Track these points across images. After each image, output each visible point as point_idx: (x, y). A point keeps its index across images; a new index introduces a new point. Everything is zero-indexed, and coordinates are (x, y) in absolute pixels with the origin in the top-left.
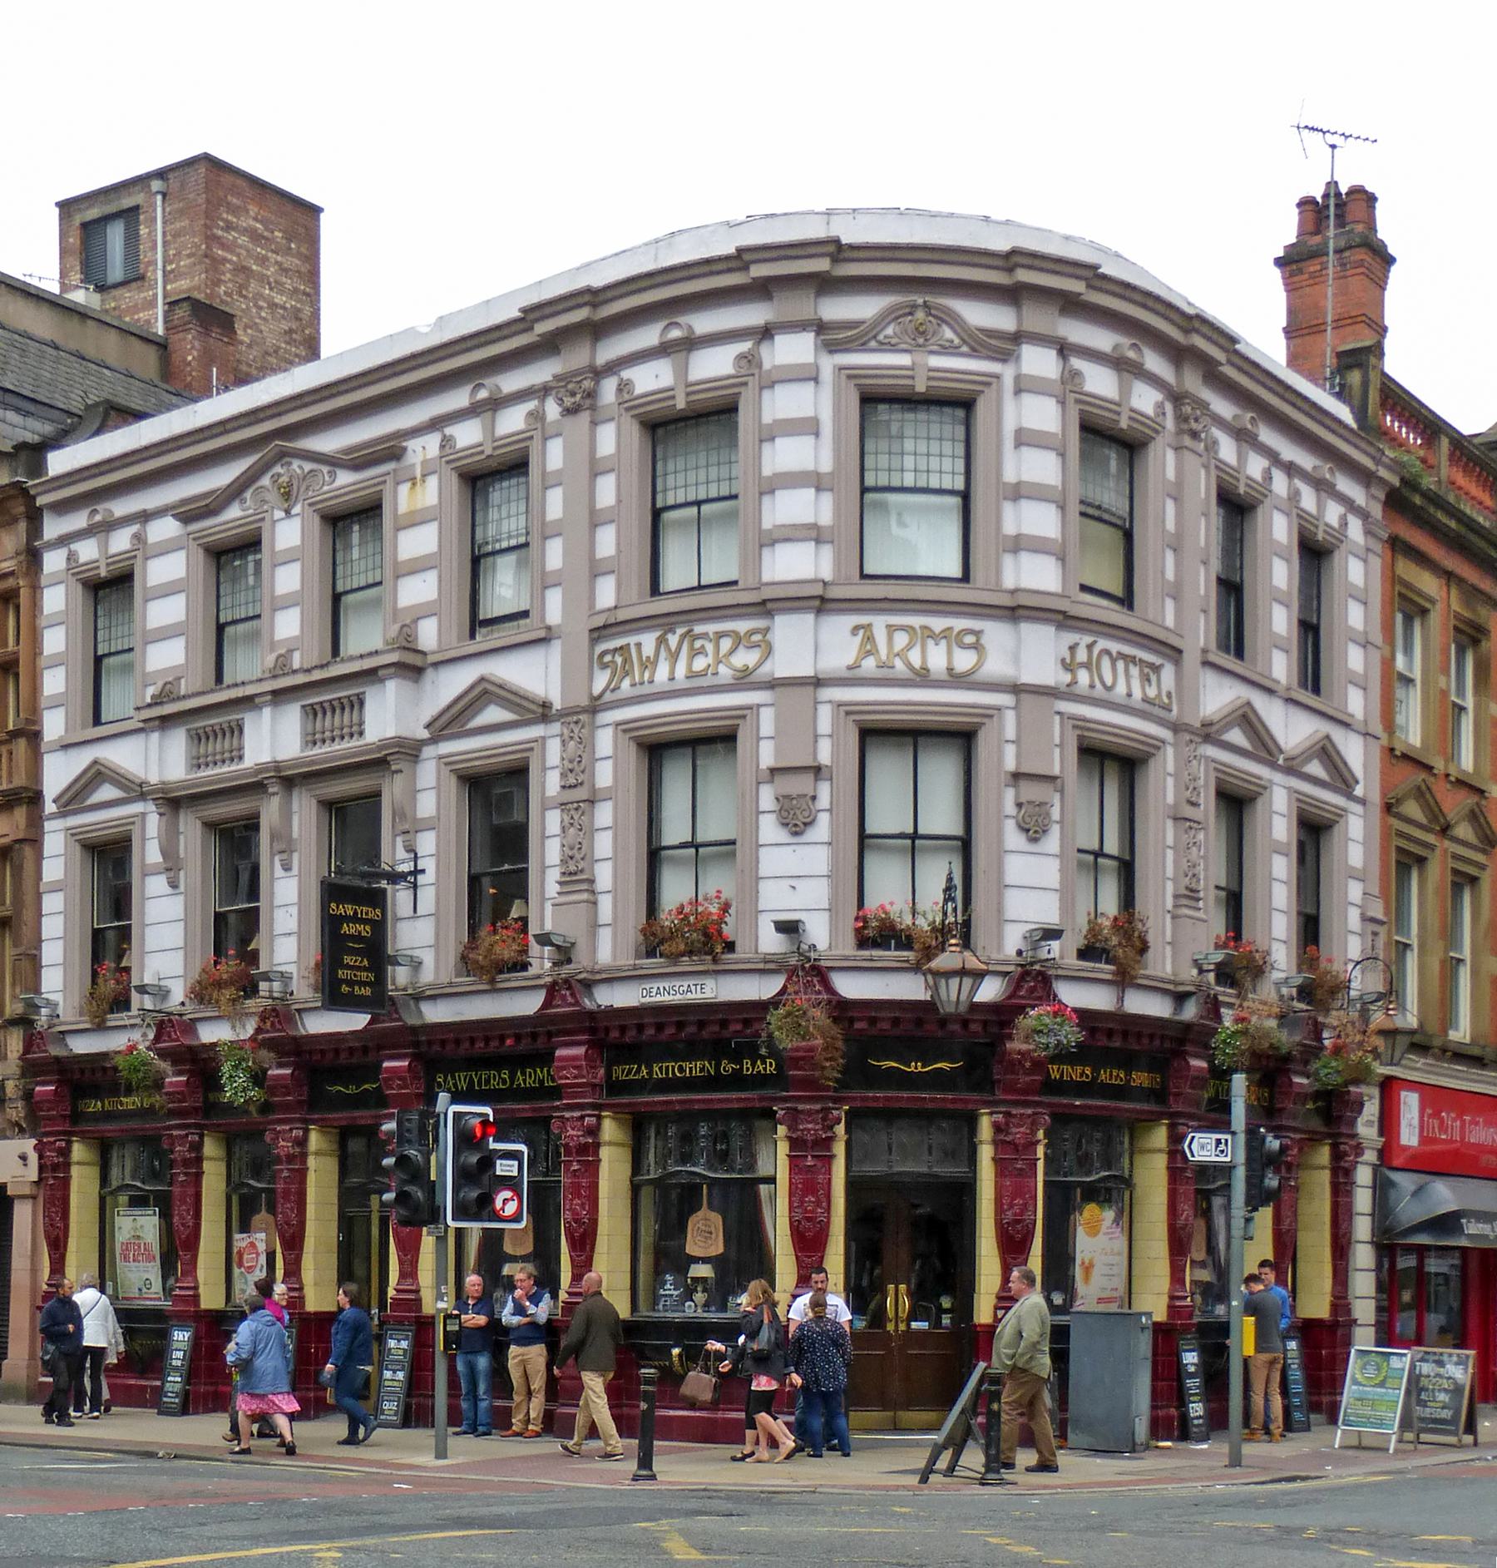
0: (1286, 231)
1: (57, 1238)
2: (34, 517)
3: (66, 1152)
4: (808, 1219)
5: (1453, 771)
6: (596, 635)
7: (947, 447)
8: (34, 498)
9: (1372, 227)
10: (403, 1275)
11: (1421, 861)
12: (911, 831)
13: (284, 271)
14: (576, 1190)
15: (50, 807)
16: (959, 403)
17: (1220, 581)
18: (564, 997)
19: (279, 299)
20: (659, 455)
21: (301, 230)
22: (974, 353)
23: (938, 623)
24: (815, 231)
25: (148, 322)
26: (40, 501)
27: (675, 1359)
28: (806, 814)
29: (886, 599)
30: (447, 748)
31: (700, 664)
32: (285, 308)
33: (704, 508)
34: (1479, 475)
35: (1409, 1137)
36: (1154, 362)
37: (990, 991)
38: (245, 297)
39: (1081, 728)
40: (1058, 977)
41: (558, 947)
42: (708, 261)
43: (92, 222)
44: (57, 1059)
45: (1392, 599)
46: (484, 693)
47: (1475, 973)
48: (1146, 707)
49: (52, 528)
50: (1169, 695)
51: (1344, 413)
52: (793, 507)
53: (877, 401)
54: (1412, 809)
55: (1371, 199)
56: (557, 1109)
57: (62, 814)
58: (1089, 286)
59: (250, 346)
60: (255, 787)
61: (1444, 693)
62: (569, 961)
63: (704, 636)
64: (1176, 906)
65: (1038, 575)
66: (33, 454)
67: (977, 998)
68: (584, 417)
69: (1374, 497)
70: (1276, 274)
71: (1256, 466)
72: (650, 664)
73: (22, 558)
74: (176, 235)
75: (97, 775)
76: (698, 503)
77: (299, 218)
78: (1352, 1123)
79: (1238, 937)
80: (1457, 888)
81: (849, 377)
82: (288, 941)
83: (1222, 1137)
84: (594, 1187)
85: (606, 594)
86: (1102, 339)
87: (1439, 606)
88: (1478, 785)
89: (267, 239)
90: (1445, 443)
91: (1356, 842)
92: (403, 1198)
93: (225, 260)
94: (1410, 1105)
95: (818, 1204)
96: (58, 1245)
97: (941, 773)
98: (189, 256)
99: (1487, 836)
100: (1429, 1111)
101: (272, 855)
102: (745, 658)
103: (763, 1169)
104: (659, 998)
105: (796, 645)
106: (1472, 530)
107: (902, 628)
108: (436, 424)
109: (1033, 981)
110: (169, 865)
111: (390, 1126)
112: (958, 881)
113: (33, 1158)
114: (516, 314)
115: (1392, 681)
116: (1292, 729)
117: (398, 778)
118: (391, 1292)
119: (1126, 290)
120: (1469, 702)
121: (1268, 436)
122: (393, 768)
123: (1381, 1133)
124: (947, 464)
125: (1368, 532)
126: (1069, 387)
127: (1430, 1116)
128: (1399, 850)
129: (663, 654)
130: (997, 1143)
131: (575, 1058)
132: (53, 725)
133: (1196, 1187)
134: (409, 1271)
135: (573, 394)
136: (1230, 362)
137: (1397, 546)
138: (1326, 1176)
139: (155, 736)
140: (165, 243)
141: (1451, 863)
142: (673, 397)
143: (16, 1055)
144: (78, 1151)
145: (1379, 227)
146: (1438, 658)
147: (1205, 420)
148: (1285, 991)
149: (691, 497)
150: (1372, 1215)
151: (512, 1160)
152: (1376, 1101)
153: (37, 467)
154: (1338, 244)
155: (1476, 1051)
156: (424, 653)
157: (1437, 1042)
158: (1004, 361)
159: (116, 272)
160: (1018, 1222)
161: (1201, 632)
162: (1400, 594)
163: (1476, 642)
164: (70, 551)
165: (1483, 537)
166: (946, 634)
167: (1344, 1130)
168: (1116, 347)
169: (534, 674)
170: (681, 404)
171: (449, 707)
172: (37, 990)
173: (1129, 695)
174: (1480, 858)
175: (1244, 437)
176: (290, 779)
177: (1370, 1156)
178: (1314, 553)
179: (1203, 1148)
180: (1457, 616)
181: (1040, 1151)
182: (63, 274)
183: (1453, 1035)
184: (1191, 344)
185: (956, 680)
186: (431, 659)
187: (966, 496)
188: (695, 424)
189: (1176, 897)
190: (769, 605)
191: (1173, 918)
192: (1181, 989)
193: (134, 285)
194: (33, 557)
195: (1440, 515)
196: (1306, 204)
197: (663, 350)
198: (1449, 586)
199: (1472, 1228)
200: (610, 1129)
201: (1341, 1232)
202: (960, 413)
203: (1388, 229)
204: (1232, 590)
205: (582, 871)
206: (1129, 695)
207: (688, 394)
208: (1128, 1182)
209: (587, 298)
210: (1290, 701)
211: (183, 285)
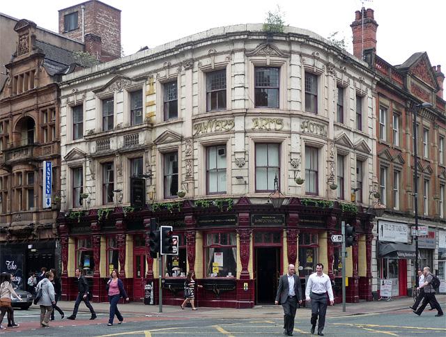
0: (353, 18)
2: (59, 91)
9: (373, 18)
12: (266, 165)
14: (190, 249)
15: (63, 159)
22: (280, 56)
26: (61, 87)
36: (321, 56)
49: (64, 93)
54: (384, 156)
55: (373, 11)
60: (113, 155)
66: (59, 76)
68: (191, 70)
70: (351, 29)
71: (345, 78)
79: (342, 121)
80: (395, 174)
84: (194, 248)
85: (196, 111)
86: (309, 52)
91: (371, 166)
93: (99, 24)
97: (273, 154)
102: (228, 127)
103: (233, 244)
105: (239, 124)
112: (278, 177)
115: (380, 127)
119: (315, 41)
120: (397, 130)
130: (287, 237)
132: (64, 141)
133: (334, 250)
134: (151, 268)
137: (379, 94)
138: (365, 243)
144: (198, 235)
151: (176, 239)
154: (365, 22)
159: (72, 28)
161: (333, 118)
164: (68, 97)
169: (177, 129)
174: (401, 166)
176: (121, 153)
178: (360, 97)
179: (335, 238)
184: (333, 51)
185: (277, 131)
194: (59, 101)
200: (198, 235)
202: (277, 69)
203: (376, 18)
204: (341, 108)
208: (318, 246)
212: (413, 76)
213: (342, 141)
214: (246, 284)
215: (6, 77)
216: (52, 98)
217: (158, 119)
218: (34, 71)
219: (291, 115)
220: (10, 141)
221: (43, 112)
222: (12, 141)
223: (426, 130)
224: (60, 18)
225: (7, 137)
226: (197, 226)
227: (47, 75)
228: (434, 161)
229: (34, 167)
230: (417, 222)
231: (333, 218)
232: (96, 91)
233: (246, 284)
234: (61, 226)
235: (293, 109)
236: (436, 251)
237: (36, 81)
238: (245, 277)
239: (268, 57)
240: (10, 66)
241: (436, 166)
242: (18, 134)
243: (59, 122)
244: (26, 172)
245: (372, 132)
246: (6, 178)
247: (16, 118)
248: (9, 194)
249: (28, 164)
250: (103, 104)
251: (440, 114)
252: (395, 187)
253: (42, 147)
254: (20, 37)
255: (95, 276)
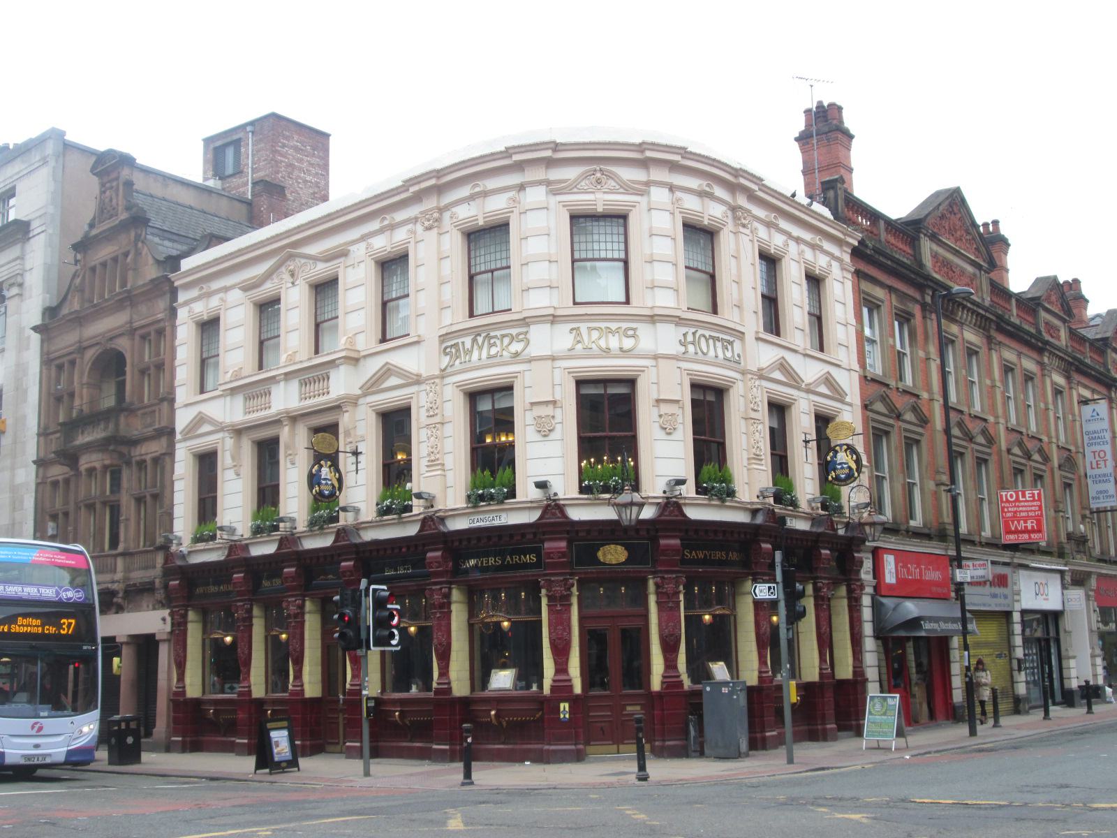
1: (180, 662)
2: (174, 292)
3: (185, 616)
4: (559, 639)
5: (900, 385)
6: (442, 338)
7: (615, 238)
8: (173, 283)
9: (841, 122)
10: (354, 676)
11: (887, 433)
13: (311, 165)
15: (178, 437)
16: (620, 218)
17: (763, 296)
18: (430, 526)
19: (308, 178)
20: (472, 248)
21: (320, 145)
23: (614, 326)
24: (546, 139)
25: (244, 192)
27: (493, 718)
28: (549, 425)
29: (586, 315)
30: (370, 399)
31: (493, 351)
32: (311, 182)
33: (495, 273)
34: (903, 238)
35: (890, 578)
36: (719, 192)
37: (648, 513)
38: (291, 178)
39: (691, 375)
40: (685, 504)
41: (426, 499)
42: (492, 154)
43: (221, 150)
44: (180, 567)
45: (860, 301)
46: (387, 371)
47: (922, 489)
48: (728, 363)
49: (182, 297)
50: (739, 356)
51: (826, 212)
52: (538, 273)
53: (580, 219)
54: (879, 406)
56: (429, 584)
57: (185, 440)
58: (682, 157)
59: (293, 201)
60: (277, 422)
61: (894, 346)
62: (432, 506)
63: (495, 337)
64: (749, 464)
65: (665, 301)
66: (173, 262)
67: (641, 517)
68: (435, 231)
69: (845, 251)
72: (470, 352)
73: (167, 312)
74: (258, 151)
75: (201, 420)
76: (492, 271)
77: (318, 140)
78: (858, 572)
81: (564, 206)
82: (294, 502)
83: (772, 585)
85: (448, 318)
86: (694, 183)
87: (886, 303)
88: (915, 392)
89: (302, 150)
90: (882, 223)
92: (342, 635)
93: (282, 161)
94: (889, 562)
95: (564, 630)
96: (181, 665)
98: (264, 161)
99: (922, 419)
100: (900, 564)
101: (286, 457)
102: (516, 347)
104: (478, 524)
105: (543, 340)
106: (900, 265)
107: (595, 329)
108: (363, 238)
109: (671, 506)
110: (235, 464)
111: (337, 598)
113: (169, 619)
114: (401, 184)
116: (810, 371)
117: (346, 415)
118: (348, 686)
120: (908, 351)
121: (783, 224)
122: (344, 410)
123: (874, 578)
124: (616, 246)
125: (843, 269)
126: (676, 206)
127: (902, 567)
128: (873, 427)
129: (475, 347)
130: (658, 594)
131: (436, 557)
132: (183, 394)
135: (429, 220)
136: (760, 189)
137: (858, 274)
138: (845, 602)
139: (228, 398)
140: (253, 155)
141: (904, 434)
142: (477, 220)
143: (160, 565)
144: (456, 595)
145: (845, 121)
146: (888, 329)
147: (749, 218)
148: (813, 505)
149: (488, 268)
150: (873, 621)
152: (871, 561)
153: (176, 268)
154: (825, 131)
155: (926, 531)
156: (359, 351)
157: (903, 527)
158: (642, 195)
160: (672, 635)
162: (864, 299)
163: (908, 320)
165: (906, 268)
166: (617, 331)
167: (853, 577)
168: (700, 185)
169: (408, 360)
170: (481, 222)
171: (371, 378)
172: (171, 531)
173: (716, 357)
174: (920, 430)
175: (769, 225)
177: (869, 590)
178: (815, 281)
180: (896, 308)
181: (682, 597)
182: (205, 172)
183: (912, 523)
184: (737, 183)
185: (624, 352)
186: (363, 354)
187: (626, 262)
188: (488, 236)
189: (749, 459)
190: (527, 320)
191: (748, 470)
192: (755, 507)
193: (238, 176)
194: (173, 312)
195: (881, 258)
196: (808, 112)
197: (472, 197)
198: (890, 293)
199: (927, 626)
200: (456, 595)
201: (856, 632)
202: (621, 221)
203: (849, 122)
204: (771, 302)
205: (438, 459)
206: (716, 357)
207: (484, 218)
209: (434, 174)
210: (806, 355)
211: (260, 174)
212: (934, 237)
213: (777, 375)
214: (564, 706)
215: (73, 269)
216: (162, 304)
217: (367, 341)
218: (126, 255)
219: (653, 319)
220: (77, 402)
221: (143, 337)
222: (81, 402)
223: (972, 352)
224: (205, 153)
225: (72, 395)
226: (456, 574)
227: (151, 261)
228: (997, 417)
229: (121, 455)
230: (958, 551)
231: (823, 551)
232: (247, 288)
233: (564, 706)
234: (171, 583)
235: (658, 304)
236: (1016, 617)
237: (130, 274)
238: (562, 689)
239: (599, 196)
240: (82, 246)
241: (1002, 428)
242: (97, 386)
243: (173, 358)
244: (105, 467)
245: (848, 357)
246: (67, 481)
247: (90, 354)
248: (71, 517)
249: (107, 450)
250: (261, 312)
251: (1000, 317)
252: (910, 475)
253: (140, 412)
254: (103, 185)
255: (240, 694)
